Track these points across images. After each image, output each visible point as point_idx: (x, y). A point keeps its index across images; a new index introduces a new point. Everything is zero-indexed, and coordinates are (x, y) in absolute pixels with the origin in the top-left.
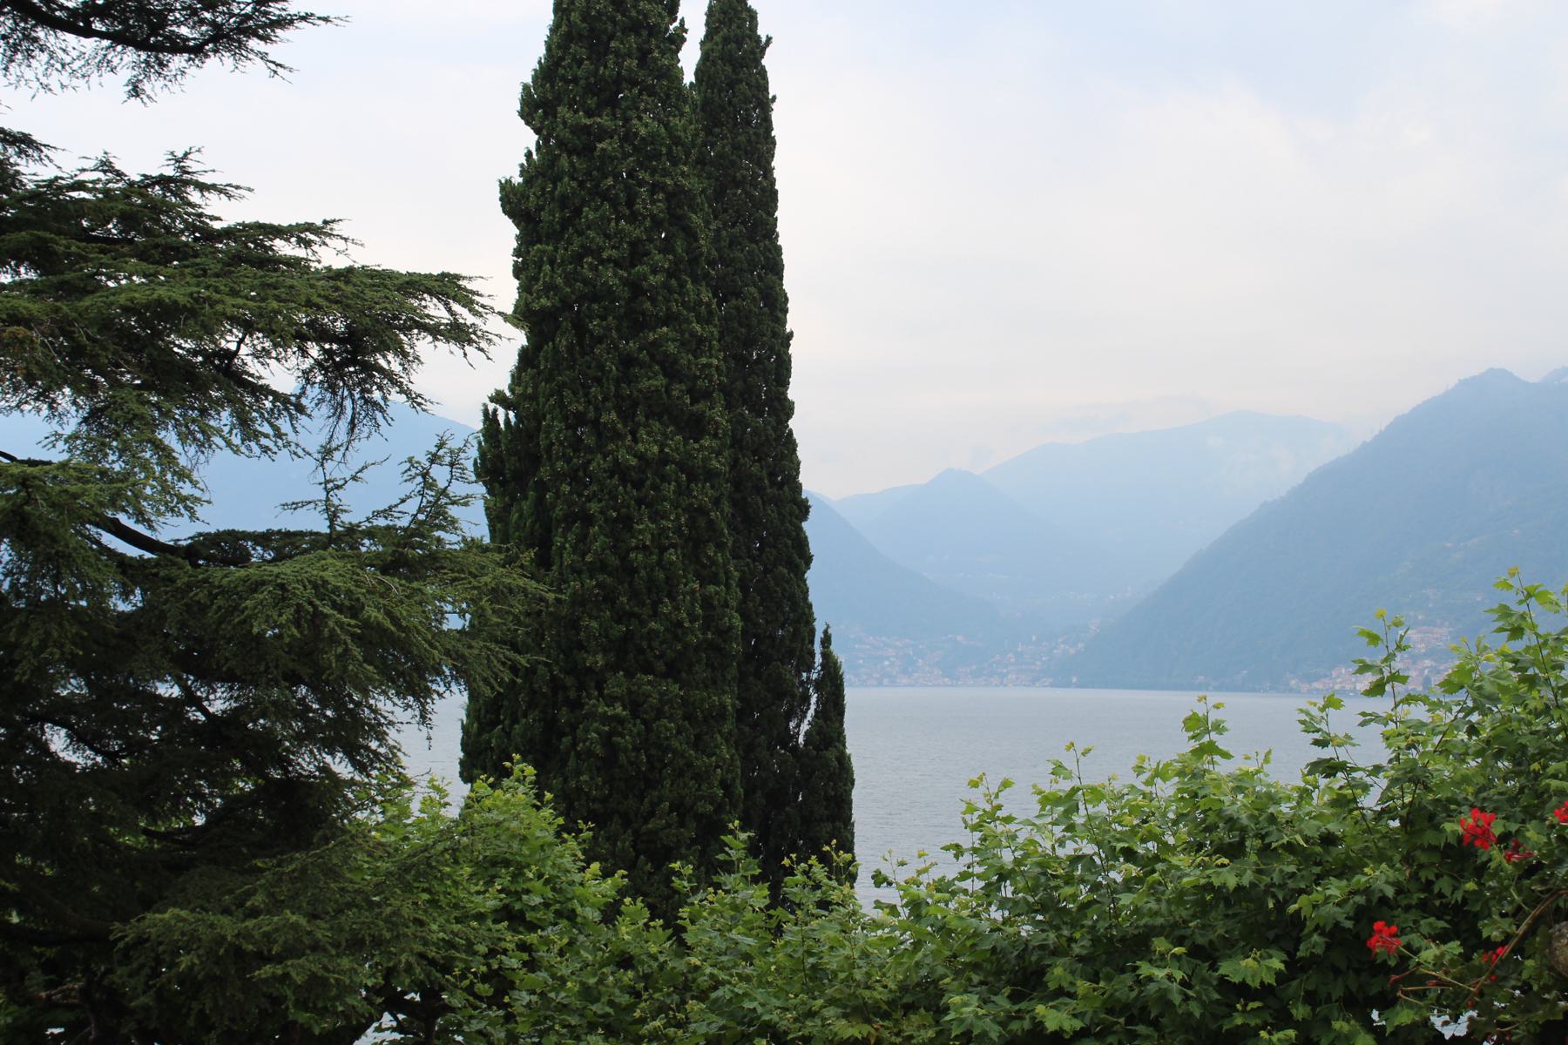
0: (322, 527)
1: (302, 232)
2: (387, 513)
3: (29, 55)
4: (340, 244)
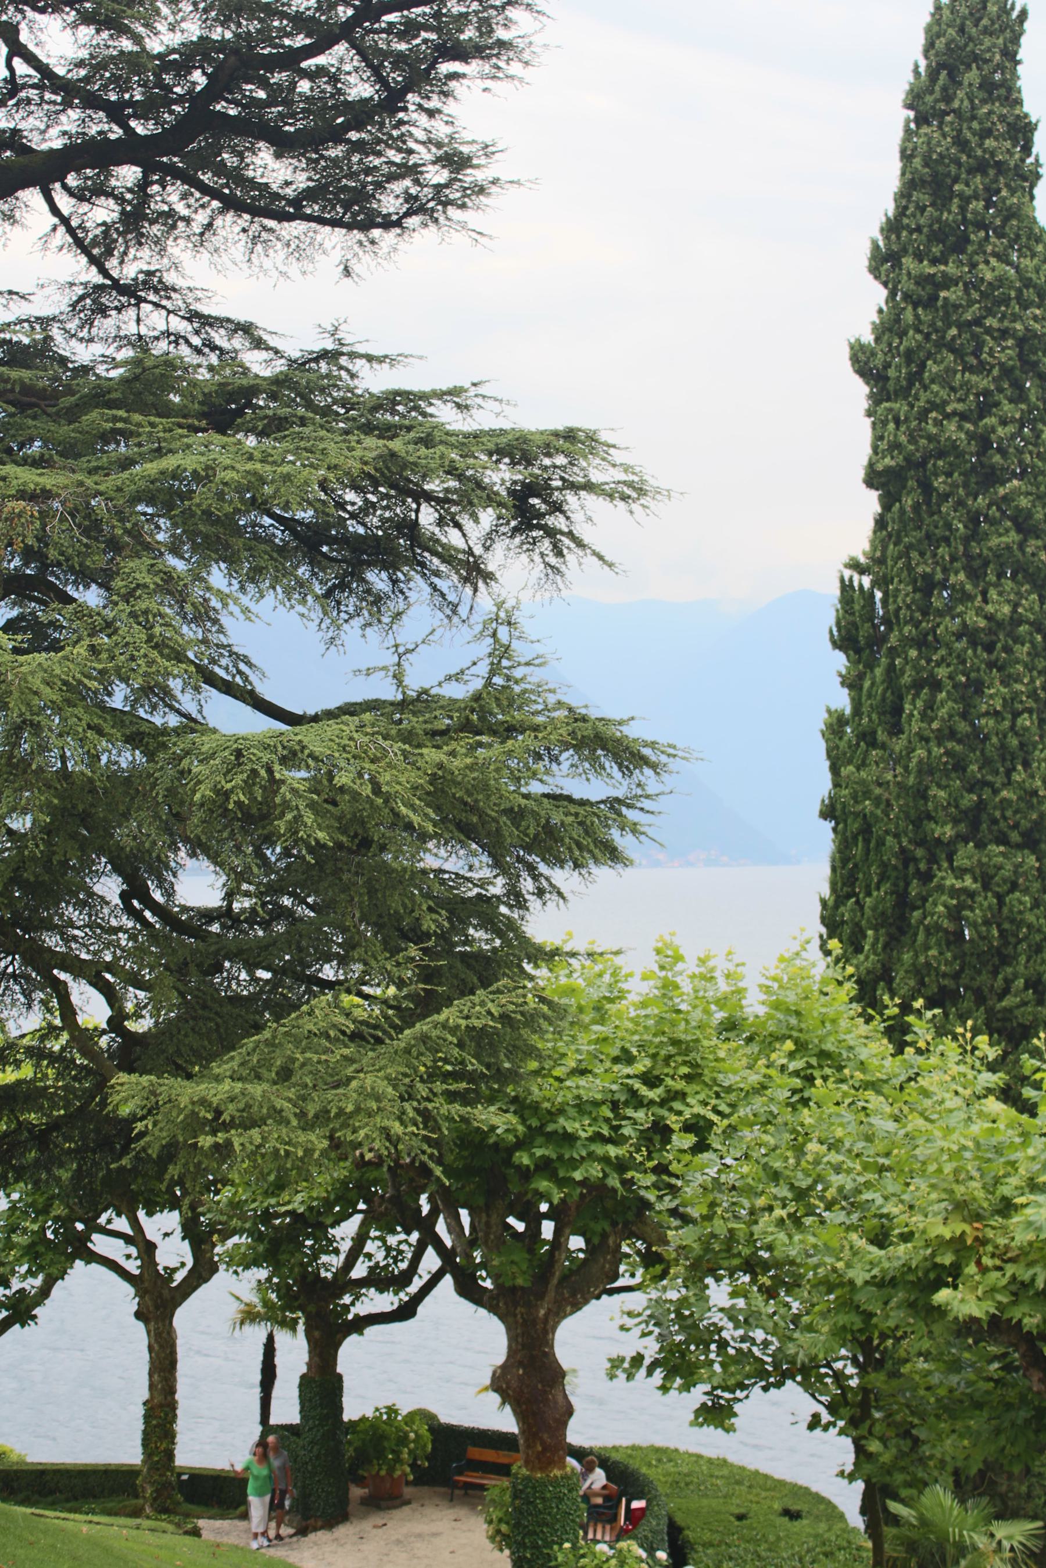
1: (452, 394)
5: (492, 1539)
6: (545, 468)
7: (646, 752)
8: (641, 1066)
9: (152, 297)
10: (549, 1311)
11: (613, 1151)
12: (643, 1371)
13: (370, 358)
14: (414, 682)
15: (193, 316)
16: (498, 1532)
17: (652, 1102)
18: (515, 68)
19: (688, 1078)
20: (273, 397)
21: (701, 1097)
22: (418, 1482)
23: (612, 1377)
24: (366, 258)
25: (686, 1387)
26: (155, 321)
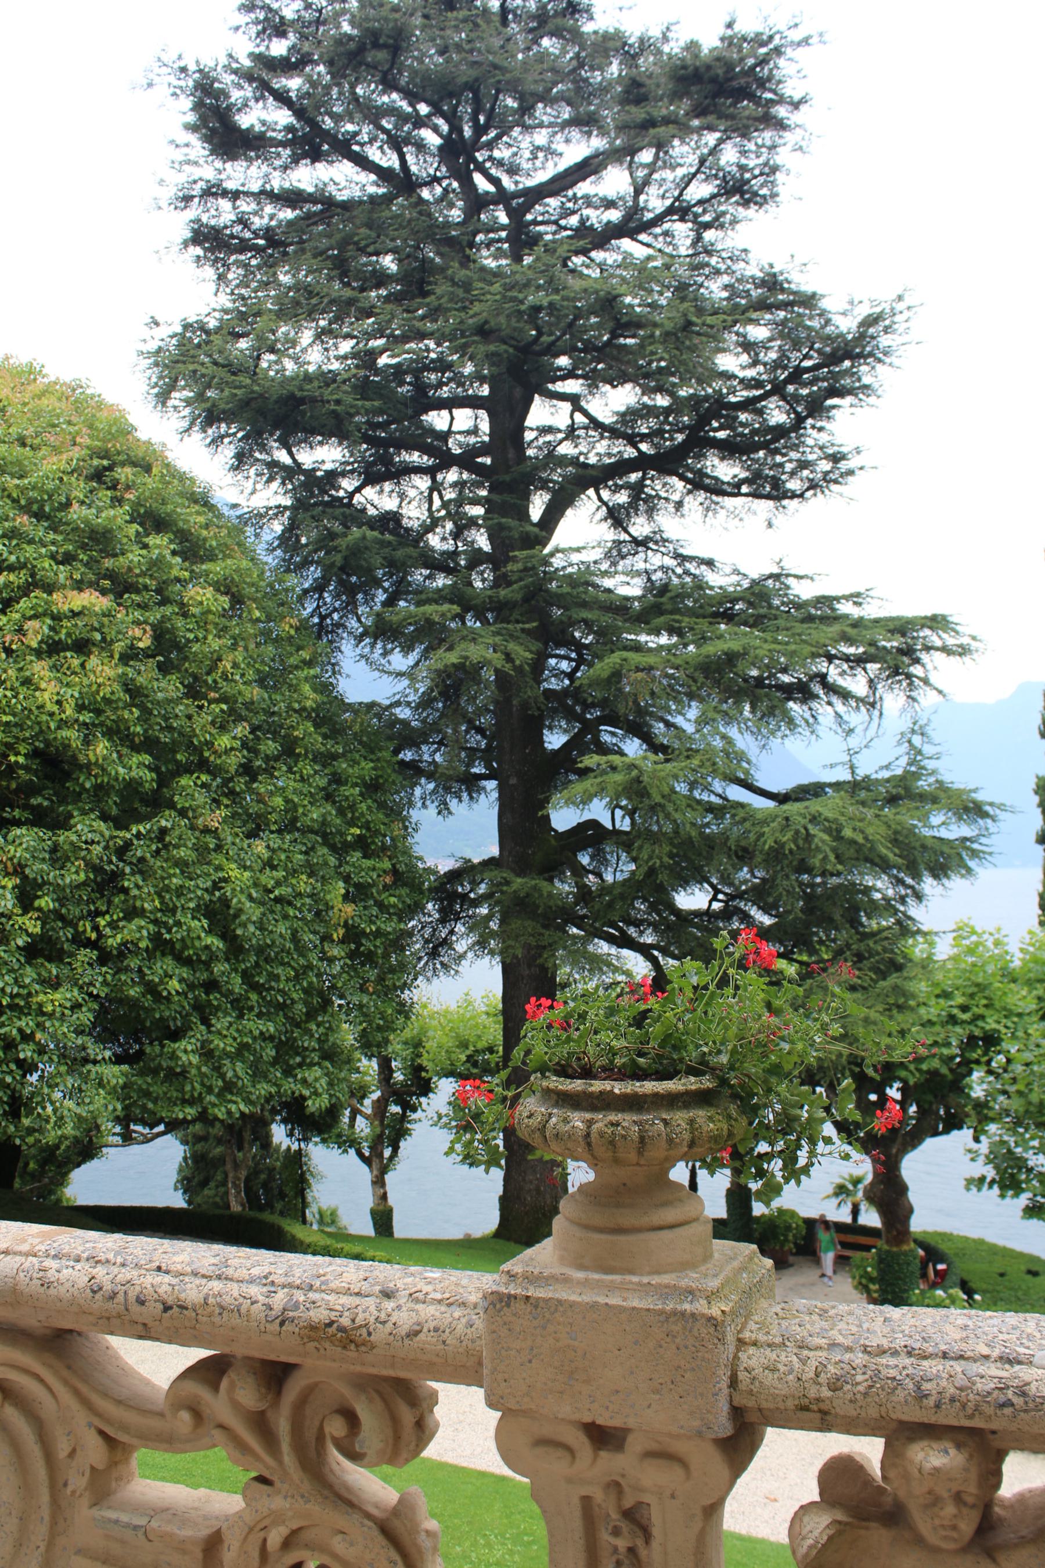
0: (848, 777)
1: (855, 598)
2: (887, 767)
3: (715, 512)
4: (878, 602)
5: (856, 1288)
6: (913, 638)
7: (987, 808)
8: (960, 1000)
9: (655, 547)
10: (898, 1150)
11: (945, 1051)
12: (986, 1186)
13: (799, 577)
14: (861, 773)
15: (677, 556)
16: (860, 1283)
17: (963, 1022)
18: (872, 400)
19: (986, 1006)
20: (815, 607)
21: (995, 1018)
22: (797, 1254)
23: (968, 1189)
24: (780, 516)
25: (1016, 1195)
26: (656, 560)
